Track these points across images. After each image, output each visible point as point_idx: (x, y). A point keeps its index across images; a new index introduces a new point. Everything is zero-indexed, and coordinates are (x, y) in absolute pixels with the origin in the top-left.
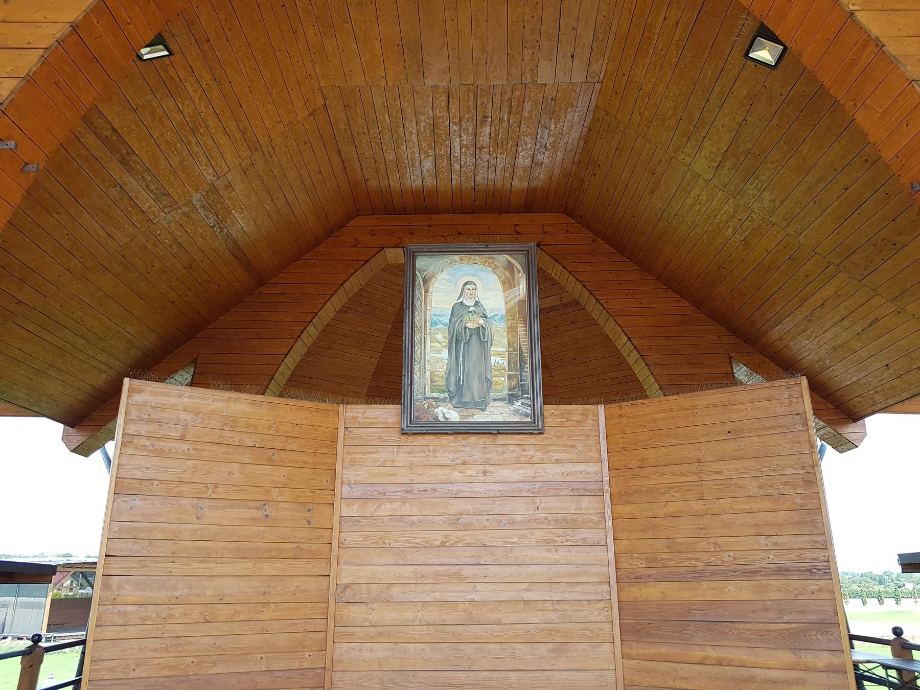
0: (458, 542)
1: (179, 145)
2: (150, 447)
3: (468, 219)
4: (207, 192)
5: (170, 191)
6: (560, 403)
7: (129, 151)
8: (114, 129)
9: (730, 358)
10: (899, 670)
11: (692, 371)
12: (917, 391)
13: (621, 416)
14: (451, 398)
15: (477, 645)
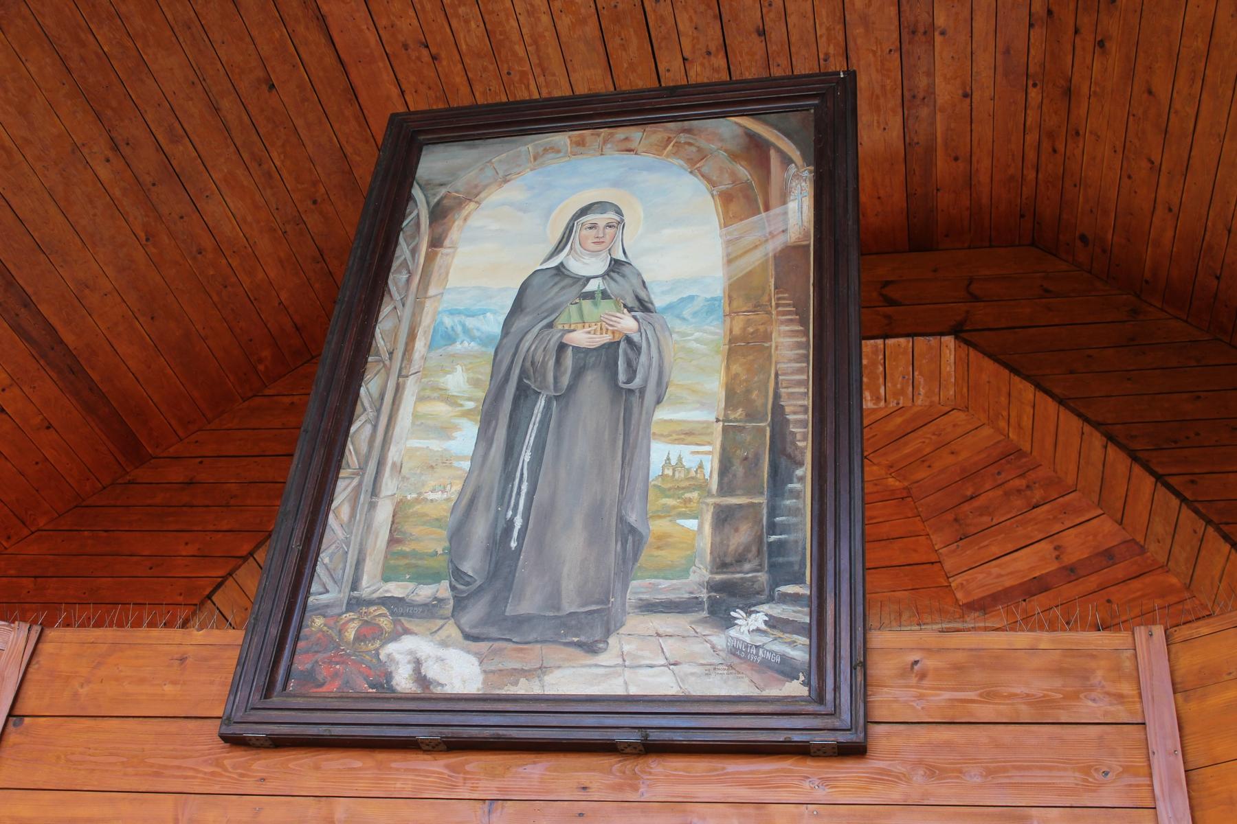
14: (460, 603)
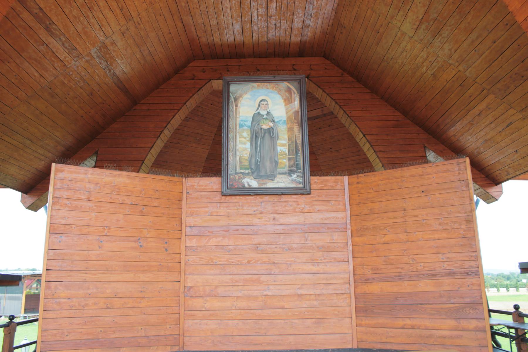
0: (258, 261)
1: (81, 18)
2: (69, 205)
3: (262, 61)
4: (100, 47)
5: (77, 47)
6: (320, 176)
7: (51, 22)
8: (40, 9)
9: (425, 147)
10: (516, 329)
11: (402, 155)
12: (526, 169)
13: (358, 183)
14: (253, 173)
15: (269, 321)
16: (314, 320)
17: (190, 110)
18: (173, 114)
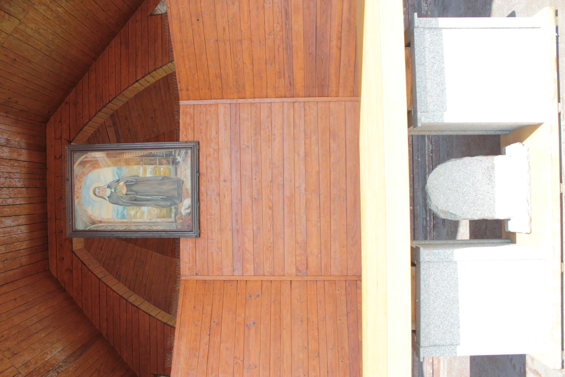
3: (49, 194)
6: (179, 130)
9: (151, 15)
11: (160, 40)
13: (187, 90)
14: (175, 204)
15: (332, 186)
16: (331, 141)
17: (107, 273)
18: (112, 292)
